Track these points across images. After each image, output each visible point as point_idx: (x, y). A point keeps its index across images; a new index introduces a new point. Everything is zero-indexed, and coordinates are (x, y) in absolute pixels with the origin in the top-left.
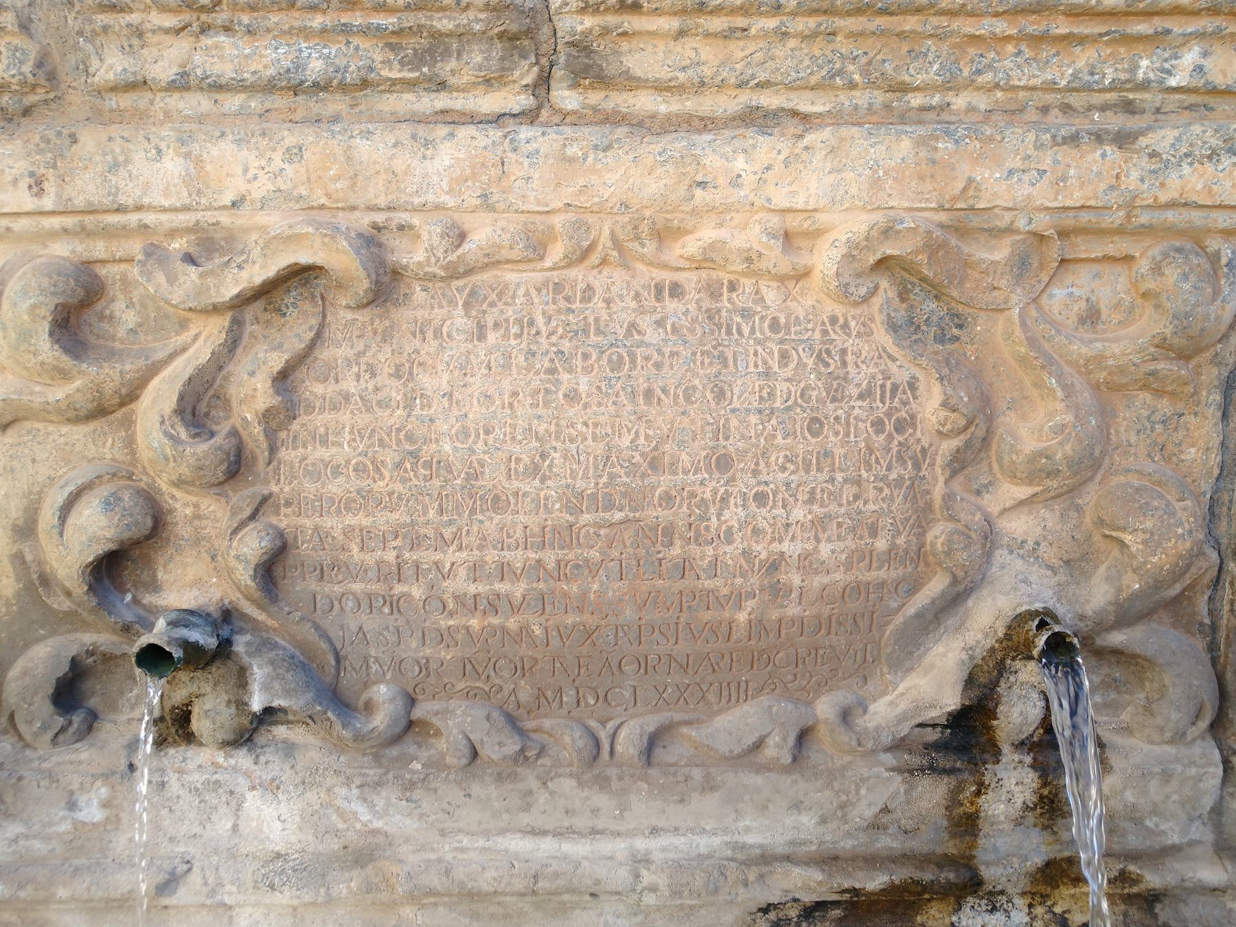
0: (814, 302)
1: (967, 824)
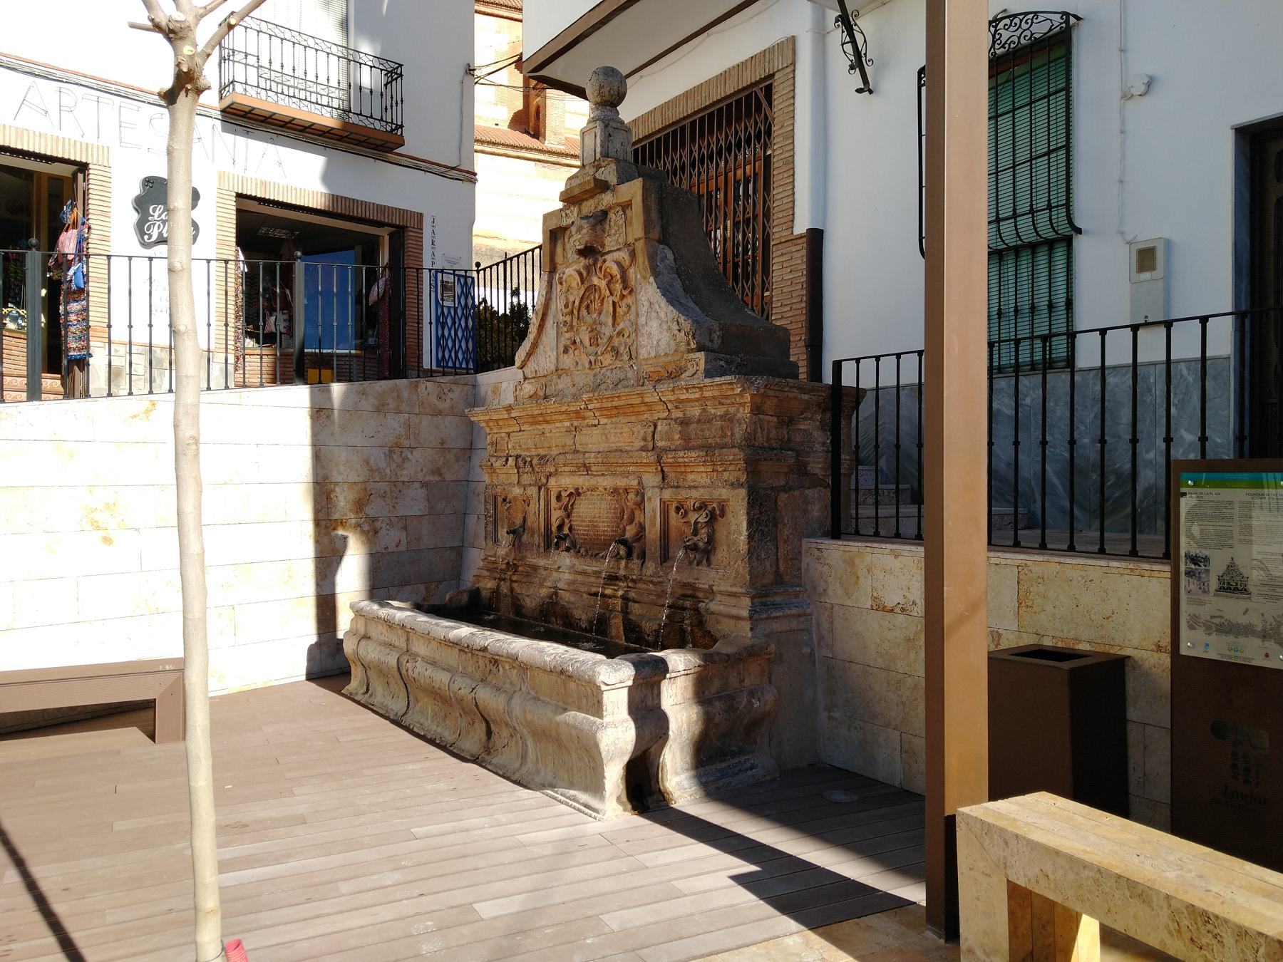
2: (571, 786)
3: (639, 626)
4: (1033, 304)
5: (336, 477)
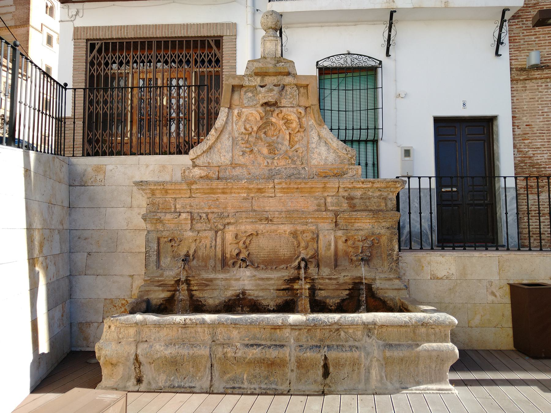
0: (287, 235)
1: (299, 274)
2: (418, 383)
3: (324, 303)
4: (367, 163)
5: (34, 226)
